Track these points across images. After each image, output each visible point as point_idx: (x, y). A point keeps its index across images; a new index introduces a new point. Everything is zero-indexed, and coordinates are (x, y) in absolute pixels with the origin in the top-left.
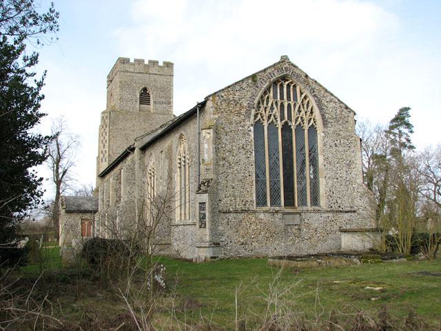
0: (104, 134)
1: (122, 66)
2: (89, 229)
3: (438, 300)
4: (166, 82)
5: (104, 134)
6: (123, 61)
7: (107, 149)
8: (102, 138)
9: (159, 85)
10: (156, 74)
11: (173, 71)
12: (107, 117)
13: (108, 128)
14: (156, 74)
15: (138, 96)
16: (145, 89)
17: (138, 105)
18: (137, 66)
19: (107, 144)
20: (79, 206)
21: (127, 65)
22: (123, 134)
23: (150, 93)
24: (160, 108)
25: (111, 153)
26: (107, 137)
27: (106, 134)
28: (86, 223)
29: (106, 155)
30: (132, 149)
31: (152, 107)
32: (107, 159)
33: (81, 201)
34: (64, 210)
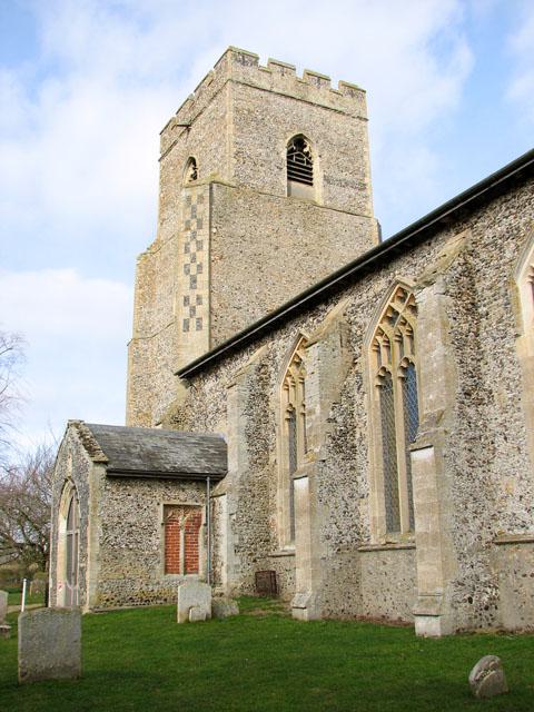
0: (193, 248)
1: (240, 69)
2: (191, 546)
3: (532, 557)
4: (249, 110)
5: (193, 248)
6: (246, 59)
7: (204, 292)
8: (187, 259)
9: (335, 137)
10: (326, 108)
11: (364, 108)
12: (201, 198)
13: (205, 231)
14: (326, 108)
15: (284, 155)
16: (299, 142)
17: (284, 181)
18: (277, 77)
19: (203, 278)
20: (150, 456)
21: (251, 70)
22: (248, 252)
23: (315, 154)
24: (344, 196)
25: (215, 306)
26: (203, 257)
27: (200, 248)
28: (182, 520)
29: (202, 310)
30: (413, 353)
31: (318, 191)
32: (205, 322)
33: (150, 444)
34: (102, 471)
